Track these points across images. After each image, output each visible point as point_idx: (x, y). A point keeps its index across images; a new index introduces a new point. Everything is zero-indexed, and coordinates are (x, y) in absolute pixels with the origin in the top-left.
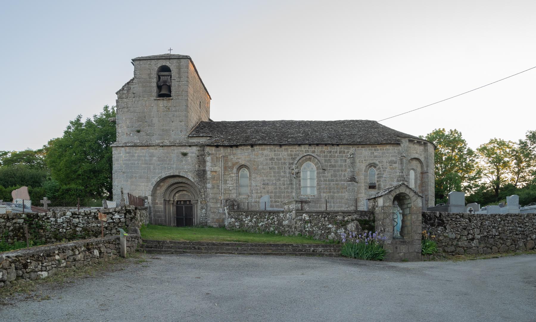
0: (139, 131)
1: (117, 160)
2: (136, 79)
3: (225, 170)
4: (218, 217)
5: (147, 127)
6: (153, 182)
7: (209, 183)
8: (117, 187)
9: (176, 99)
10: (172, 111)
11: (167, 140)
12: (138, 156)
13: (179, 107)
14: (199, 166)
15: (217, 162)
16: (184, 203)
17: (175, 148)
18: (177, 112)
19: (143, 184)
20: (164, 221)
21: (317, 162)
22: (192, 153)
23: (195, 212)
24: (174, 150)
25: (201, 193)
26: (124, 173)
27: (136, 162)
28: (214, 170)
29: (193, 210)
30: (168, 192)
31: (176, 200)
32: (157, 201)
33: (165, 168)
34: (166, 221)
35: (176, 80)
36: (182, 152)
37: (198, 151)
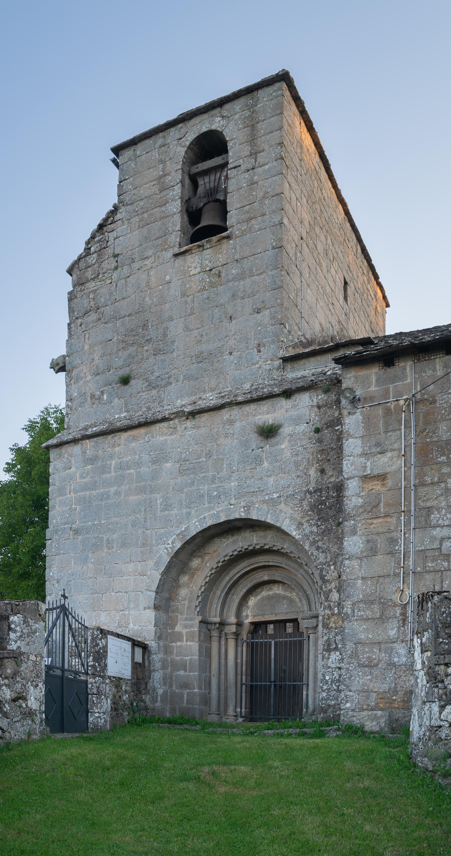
0: (125, 381)
1: (61, 491)
2: (122, 209)
3: (425, 464)
4: (385, 687)
5: (151, 360)
6: (160, 557)
7: (354, 533)
8: (56, 585)
9: (243, 233)
10: (228, 281)
11: (212, 390)
12: (120, 467)
13: (252, 258)
14: (322, 471)
15: (386, 432)
16: (275, 629)
17: (235, 412)
18: (244, 279)
19: (131, 567)
20: (198, 699)
21: (194, 632)
22: (297, 421)
23: (311, 663)
24: (231, 422)
25: (325, 582)
26: (77, 532)
27: (113, 490)
28: (376, 472)
29: (305, 657)
30: (219, 592)
31: (250, 620)
32: (178, 628)
33: (202, 496)
34: (206, 700)
35: (243, 168)
36: (261, 423)
37: (319, 407)
